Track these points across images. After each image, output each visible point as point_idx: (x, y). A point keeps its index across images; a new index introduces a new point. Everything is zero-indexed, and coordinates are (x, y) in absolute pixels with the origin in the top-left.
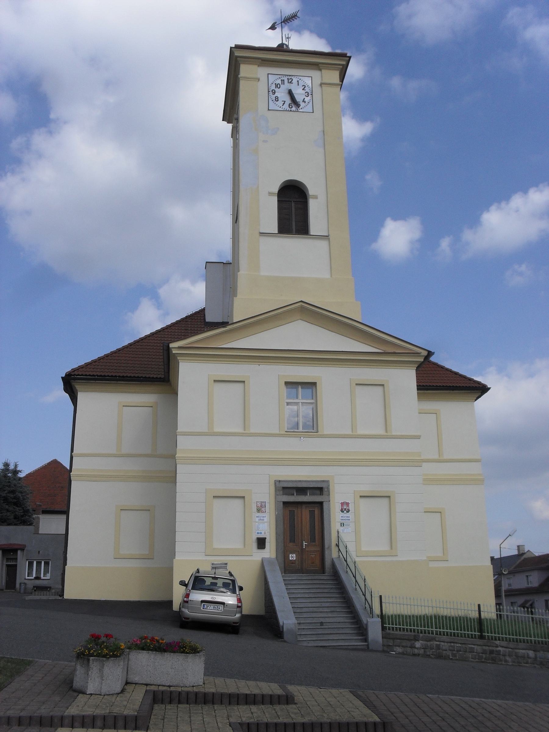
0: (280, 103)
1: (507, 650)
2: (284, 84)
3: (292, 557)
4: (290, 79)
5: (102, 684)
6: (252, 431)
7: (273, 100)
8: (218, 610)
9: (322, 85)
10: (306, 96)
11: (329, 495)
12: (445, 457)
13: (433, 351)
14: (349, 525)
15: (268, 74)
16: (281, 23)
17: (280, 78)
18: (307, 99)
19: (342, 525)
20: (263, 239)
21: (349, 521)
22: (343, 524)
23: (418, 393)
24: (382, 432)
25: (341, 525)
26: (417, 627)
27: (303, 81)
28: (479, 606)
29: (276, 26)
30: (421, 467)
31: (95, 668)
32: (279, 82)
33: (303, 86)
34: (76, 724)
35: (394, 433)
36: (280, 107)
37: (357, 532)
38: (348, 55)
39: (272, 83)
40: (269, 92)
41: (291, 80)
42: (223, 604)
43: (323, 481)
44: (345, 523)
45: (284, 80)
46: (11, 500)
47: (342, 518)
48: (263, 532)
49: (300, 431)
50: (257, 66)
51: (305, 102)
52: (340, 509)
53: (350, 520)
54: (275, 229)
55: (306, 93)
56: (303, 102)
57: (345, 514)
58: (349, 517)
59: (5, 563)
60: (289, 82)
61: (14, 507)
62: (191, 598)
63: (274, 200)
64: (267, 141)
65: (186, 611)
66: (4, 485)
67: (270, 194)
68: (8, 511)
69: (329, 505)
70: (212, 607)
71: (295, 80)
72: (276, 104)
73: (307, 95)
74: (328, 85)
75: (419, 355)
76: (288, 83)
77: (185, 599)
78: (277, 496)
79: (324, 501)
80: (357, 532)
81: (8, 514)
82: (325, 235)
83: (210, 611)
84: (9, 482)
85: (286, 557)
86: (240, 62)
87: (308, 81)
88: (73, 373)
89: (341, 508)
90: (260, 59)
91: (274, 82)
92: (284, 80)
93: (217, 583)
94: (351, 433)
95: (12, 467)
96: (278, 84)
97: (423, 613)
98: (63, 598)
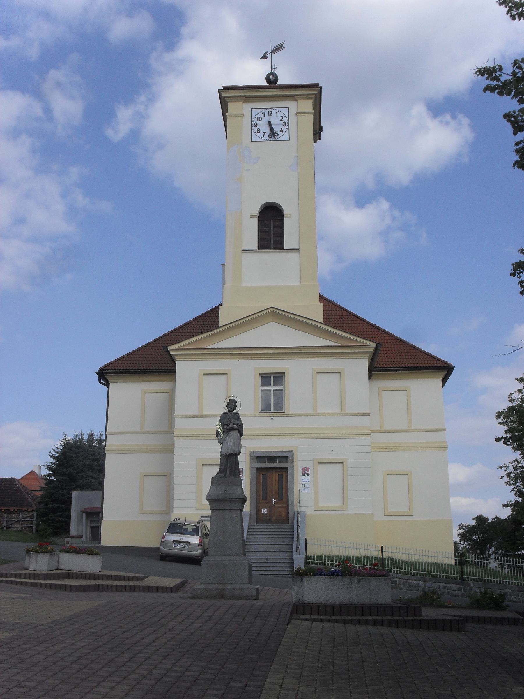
0: (261, 134)
1: (403, 580)
2: (265, 117)
3: (264, 511)
4: (270, 112)
5: (36, 565)
7: (255, 133)
8: (185, 547)
9: (297, 115)
10: (283, 126)
12: (414, 428)
14: (308, 486)
15: (252, 109)
16: (271, 52)
17: (261, 112)
18: (285, 129)
19: (303, 485)
20: (245, 256)
21: (309, 483)
22: (304, 485)
24: (337, 410)
25: (302, 486)
26: (399, 569)
27: (281, 112)
28: (382, 547)
29: (267, 56)
31: (33, 558)
33: (281, 117)
34: (13, 577)
40: (252, 125)
41: (271, 112)
42: (188, 543)
45: (265, 113)
46: (96, 468)
47: (303, 480)
49: (272, 412)
50: (242, 103)
52: (302, 473)
54: (255, 245)
55: (283, 123)
56: (281, 131)
57: (306, 477)
58: (309, 479)
59: (89, 525)
60: (269, 114)
61: (99, 474)
62: (166, 539)
64: (250, 170)
65: (162, 548)
66: (89, 454)
67: (252, 216)
68: (92, 477)
69: (293, 470)
70: (180, 545)
71: (274, 113)
72: (282, 113)
73: (284, 125)
75: (370, 346)
76: (268, 115)
77: (162, 540)
78: (252, 464)
81: (93, 480)
83: (180, 548)
84: (94, 451)
86: (227, 101)
87: (285, 112)
88: (105, 369)
89: (303, 472)
91: (256, 115)
92: (265, 113)
93: (187, 529)
95: (97, 437)
96: (260, 117)
97: (413, 560)
98: (100, 545)
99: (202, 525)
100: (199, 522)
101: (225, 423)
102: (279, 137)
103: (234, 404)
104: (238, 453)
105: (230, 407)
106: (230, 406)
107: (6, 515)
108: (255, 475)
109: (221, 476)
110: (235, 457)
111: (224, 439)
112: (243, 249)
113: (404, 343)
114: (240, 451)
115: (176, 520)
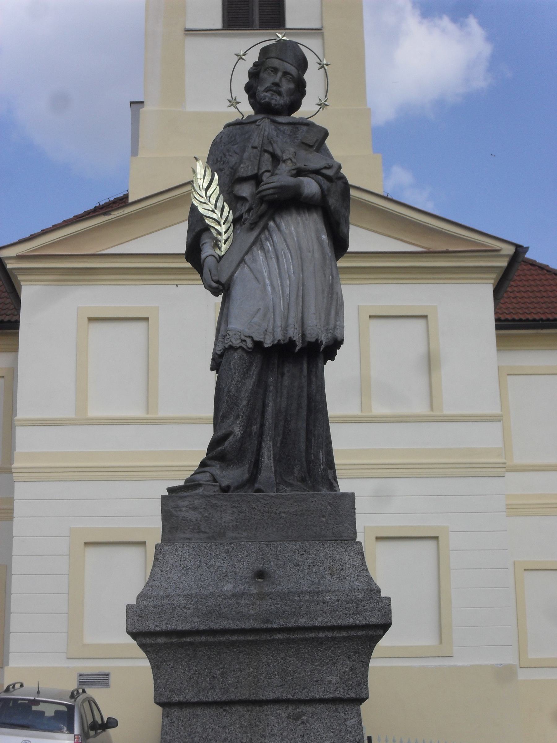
6: (161, 414)
13: (525, 245)
20: (193, 43)
23: (498, 336)
30: (503, 478)
35: (447, 411)
99: (83, 702)
100: (75, 692)
101: (246, 170)
103: (293, 70)
104: (327, 347)
105: (268, 84)
106: (269, 79)
107: (321, 600)
109: (225, 483)
110: (305, 366)
111: (242, 260)
112: (189, 27)
113: (548, 271)
114: (338, 334)
115: (14, 687)
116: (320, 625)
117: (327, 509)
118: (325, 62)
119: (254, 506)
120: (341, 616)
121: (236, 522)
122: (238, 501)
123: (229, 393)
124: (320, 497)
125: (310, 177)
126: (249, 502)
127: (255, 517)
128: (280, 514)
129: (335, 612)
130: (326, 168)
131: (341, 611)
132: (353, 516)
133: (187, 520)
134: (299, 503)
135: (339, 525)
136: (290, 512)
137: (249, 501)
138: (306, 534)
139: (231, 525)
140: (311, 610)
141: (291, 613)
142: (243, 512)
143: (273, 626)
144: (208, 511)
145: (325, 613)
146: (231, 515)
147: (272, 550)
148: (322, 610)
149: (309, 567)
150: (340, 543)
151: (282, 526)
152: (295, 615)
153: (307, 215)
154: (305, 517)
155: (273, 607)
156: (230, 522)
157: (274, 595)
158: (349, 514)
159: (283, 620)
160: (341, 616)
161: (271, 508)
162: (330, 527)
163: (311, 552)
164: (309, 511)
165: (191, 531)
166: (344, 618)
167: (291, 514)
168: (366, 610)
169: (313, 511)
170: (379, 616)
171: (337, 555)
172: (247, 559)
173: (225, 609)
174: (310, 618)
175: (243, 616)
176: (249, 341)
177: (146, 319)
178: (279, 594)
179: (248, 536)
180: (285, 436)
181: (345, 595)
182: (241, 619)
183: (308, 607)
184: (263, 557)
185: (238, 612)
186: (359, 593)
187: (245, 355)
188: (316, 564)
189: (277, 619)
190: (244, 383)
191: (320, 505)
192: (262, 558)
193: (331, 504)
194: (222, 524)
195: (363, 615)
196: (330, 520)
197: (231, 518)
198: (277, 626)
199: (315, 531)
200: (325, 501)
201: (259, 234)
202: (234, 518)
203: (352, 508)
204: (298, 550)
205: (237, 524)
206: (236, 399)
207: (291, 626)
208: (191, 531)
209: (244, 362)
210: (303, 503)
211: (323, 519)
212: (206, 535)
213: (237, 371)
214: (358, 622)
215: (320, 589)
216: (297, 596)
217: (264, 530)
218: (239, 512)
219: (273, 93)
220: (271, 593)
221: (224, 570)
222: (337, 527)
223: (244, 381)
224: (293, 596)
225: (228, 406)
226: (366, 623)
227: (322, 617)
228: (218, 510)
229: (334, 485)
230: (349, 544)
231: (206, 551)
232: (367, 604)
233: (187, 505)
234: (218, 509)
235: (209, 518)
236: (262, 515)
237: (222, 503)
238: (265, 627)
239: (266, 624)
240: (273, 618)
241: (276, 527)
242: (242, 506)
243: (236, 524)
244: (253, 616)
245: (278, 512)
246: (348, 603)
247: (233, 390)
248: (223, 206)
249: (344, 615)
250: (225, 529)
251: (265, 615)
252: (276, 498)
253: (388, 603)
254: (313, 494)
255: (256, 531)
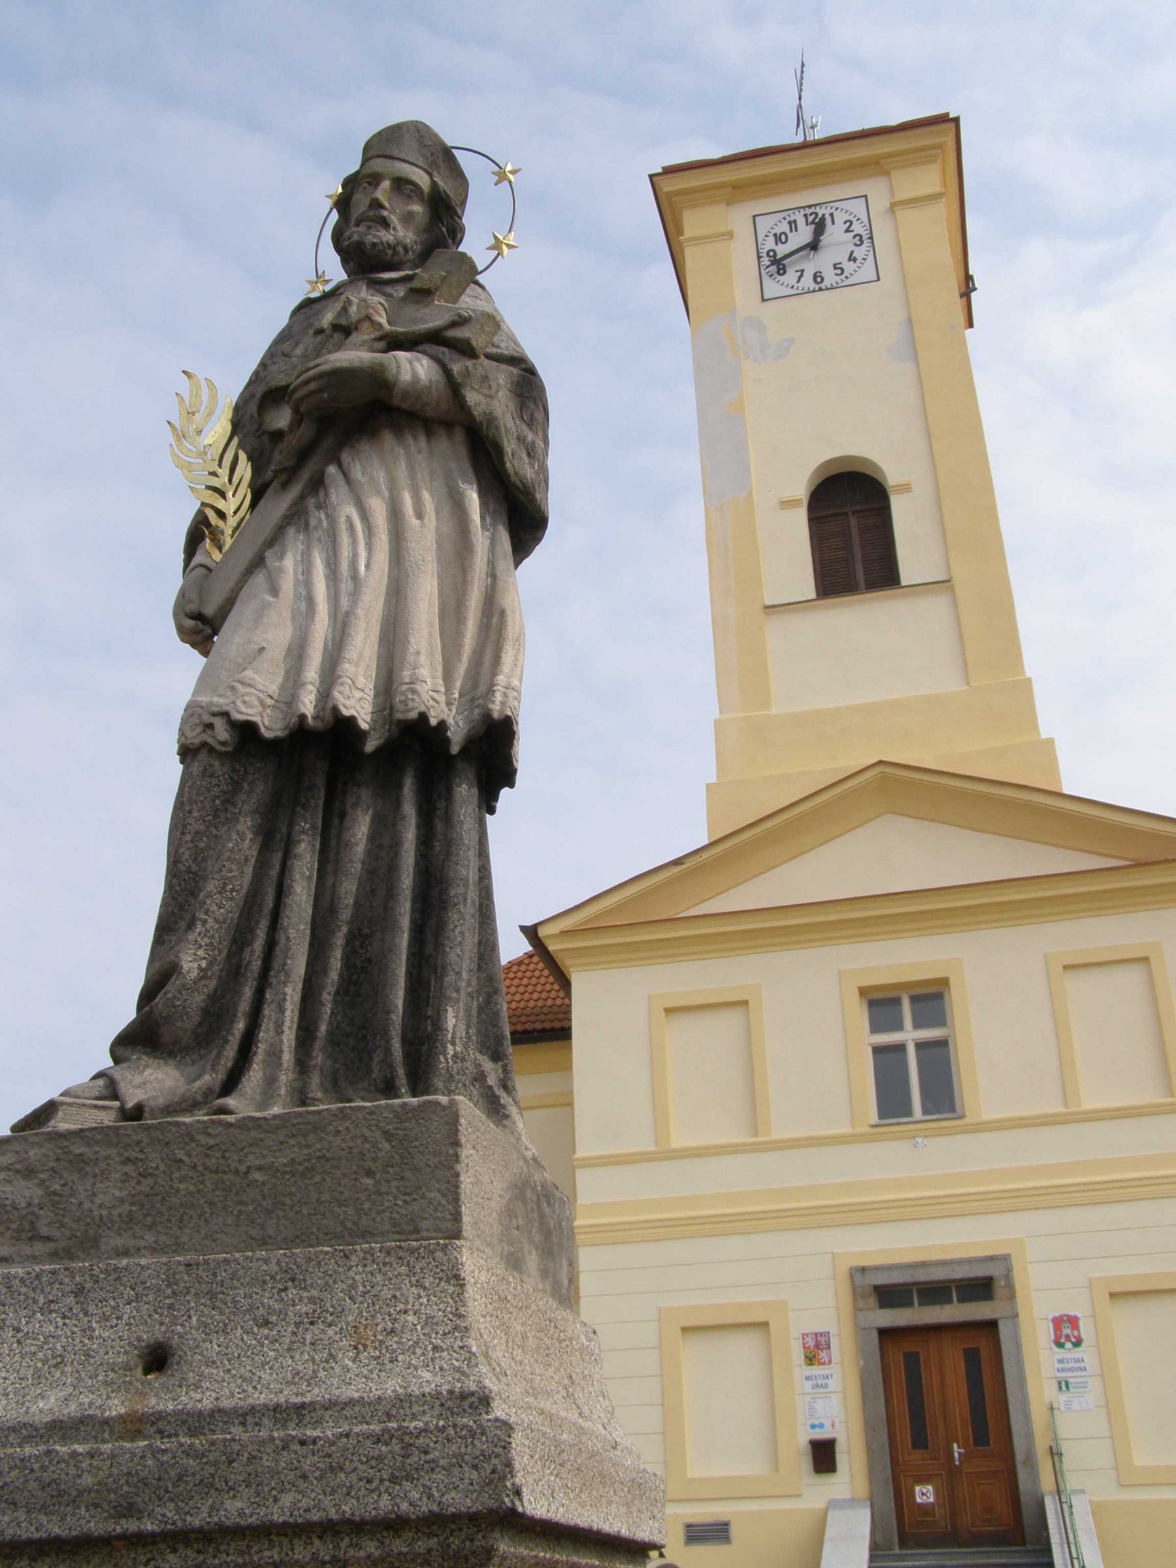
2: (796, 230)
3: (923, 1494)
4: (811, 214)
6: (775, 1136)
10: (856, 245)
11: (1012, 1297)
18: (859, 253)
19: (1063, 1385)
22: (1067, 1384)
32: (784, 227)
33: (845, 222)
36: (792, 287)
37: (1112, 1408)
38: (951, 116)
39: (864, 259)
43: (992, 1258)
44: (1070, 1380)
45: (795, 221)
48: (828, 1425)
51: (855, 260)
52: (1053, 1337)
53: (1085, 1369)
55: (854, 237)
56: (850, 259)
57: (1069, 1353)
60: (809, 221)
63: (800, 519)
67: (786, 504)
74: (909, 203)
76: (807, 224)
78: (860, 1313)
79: (1001, 1318)
80: (1112, 1408)
82: (942, 579)
85: (901, 1497)
90: (727, 186)
92: (795, 221)
94: (1062, 1110)
102: (847, 278)
108: (877, 1357)
116: (287, 1519)
117: (380, 1150)
118: (509, 168)
119: (180, 1154)
120: (351, 1486)
121: (132, 1204)
122: (138, 1143)
123: (176, 866)
124: (360, 1115)
125: (424, 353)
126: (167, 1143)
127: (181, 1186)
128: (247, 1173)
129: (335, 1475)
130: (453, 324)
131: (355, 1469)
132: (452, 1167)
133: (5, 1205)
134: (301, 1139)
135: (412, 1197)
136: (276, 1165)
137: (166, 1140)
138: (314, 1230)
139: (115, 1212)
140: (260, 1470)
141: (201, 1481)
142: (150, 1174)
143: (142, 1527)
144: (61, 1177)
145: (304, 1477)
146: (119, 1184)
147: (199, 1280)
148: (296, 1469)
149: (297, 1328)
150: (397, 1249)
151: (251, 1208)
152: (212, 1485)
153: (422, 441)
154: (317, 1178)
155: (150, 1462)
156: (114, 1207)
157: (169, 1422)
158: (439, 1162)
159: (177, 1505)
160: (351, 1486)
161: (224, 1158)
162: (386, 1204)
163: (309, 1282)
164: (328, 1160)
165: (13, 1237)
166: (363, 1492)
167: (278, 1170)
168: (433, 1465)
169: (339, 1159)
170: (471, 1484)
171: (383, 1285)
172: (129, 1311)
173: (12, 1474)
174: (258, 1495)
175: (61, 1494)
176: (219, 723)
177: (745, 1003)
178: (185, 1417)
179: (156, 1242)
180: (355, 977)
181: (380, 1414)
182: (54, 1505)
183: (254, 1457)
184: (172, 1304)
185: (47, 1481)
186: (426, 1407)
187: (217, 764)
188: (319, 1318)
189: (157, 1503)
190: (216, 836)
191: (359, 1141)
192: (171, 1307)
193: (392, 1135)
194: (92, 1211)
195: (421, 1481)
196: (388, 1181)
197: (117, 1193)
198: (155, 1527)
199: (341, 1218)
200: (374, 1128)
201: (302, 497)
202: (126, 1192)
203: (452, 1144)
204: (272, 1277)
205: (134, 1208)
206: (194, 879)
207: (197, 1523)
208: (13, 1237)
209: (215, 781)
210: (311, 1137)
211: (368, 1181)
212: (51, 1246)
213: (194, 807)
214: (404, 1506)
215: (308, 1399)
216: (236, 1421)
217: (202, 1224)
218: (140, 1174)
219: (370, 224)
220: (160, 1416)
221: (58, 1346)
222: (405, 1202)
223: (214, 832)
224: (226, 1423)
225: (174, 898)
226: (430, 1511)
227: (293, 1494)
228: (87, 1173)
229: (502, 1101)
230: (422, 1250)
231: (24, 1290)
232: (436, 1442)
233: (11, 1164)
234: (88, 1169)
235: (61, 1196)
236: (200, 1179)
237: (97, 1152)
238: (119, 1529)
239: (123, 1521)
240: (147, 1499)
241: (235, 1213)
242: (147, 1158)
243: (131, 1211)
244: (89, 1492)
245: (243, 1168)
246: (378, 1441)
247: (186, 856)
248: (236, 458)
249: (361, 1484)
250: (99, 1226)
251: (125, 1488)
252: (239, 1127)
253: (503, 1437)
254: (341, 1110)
255: (180, 1227)
